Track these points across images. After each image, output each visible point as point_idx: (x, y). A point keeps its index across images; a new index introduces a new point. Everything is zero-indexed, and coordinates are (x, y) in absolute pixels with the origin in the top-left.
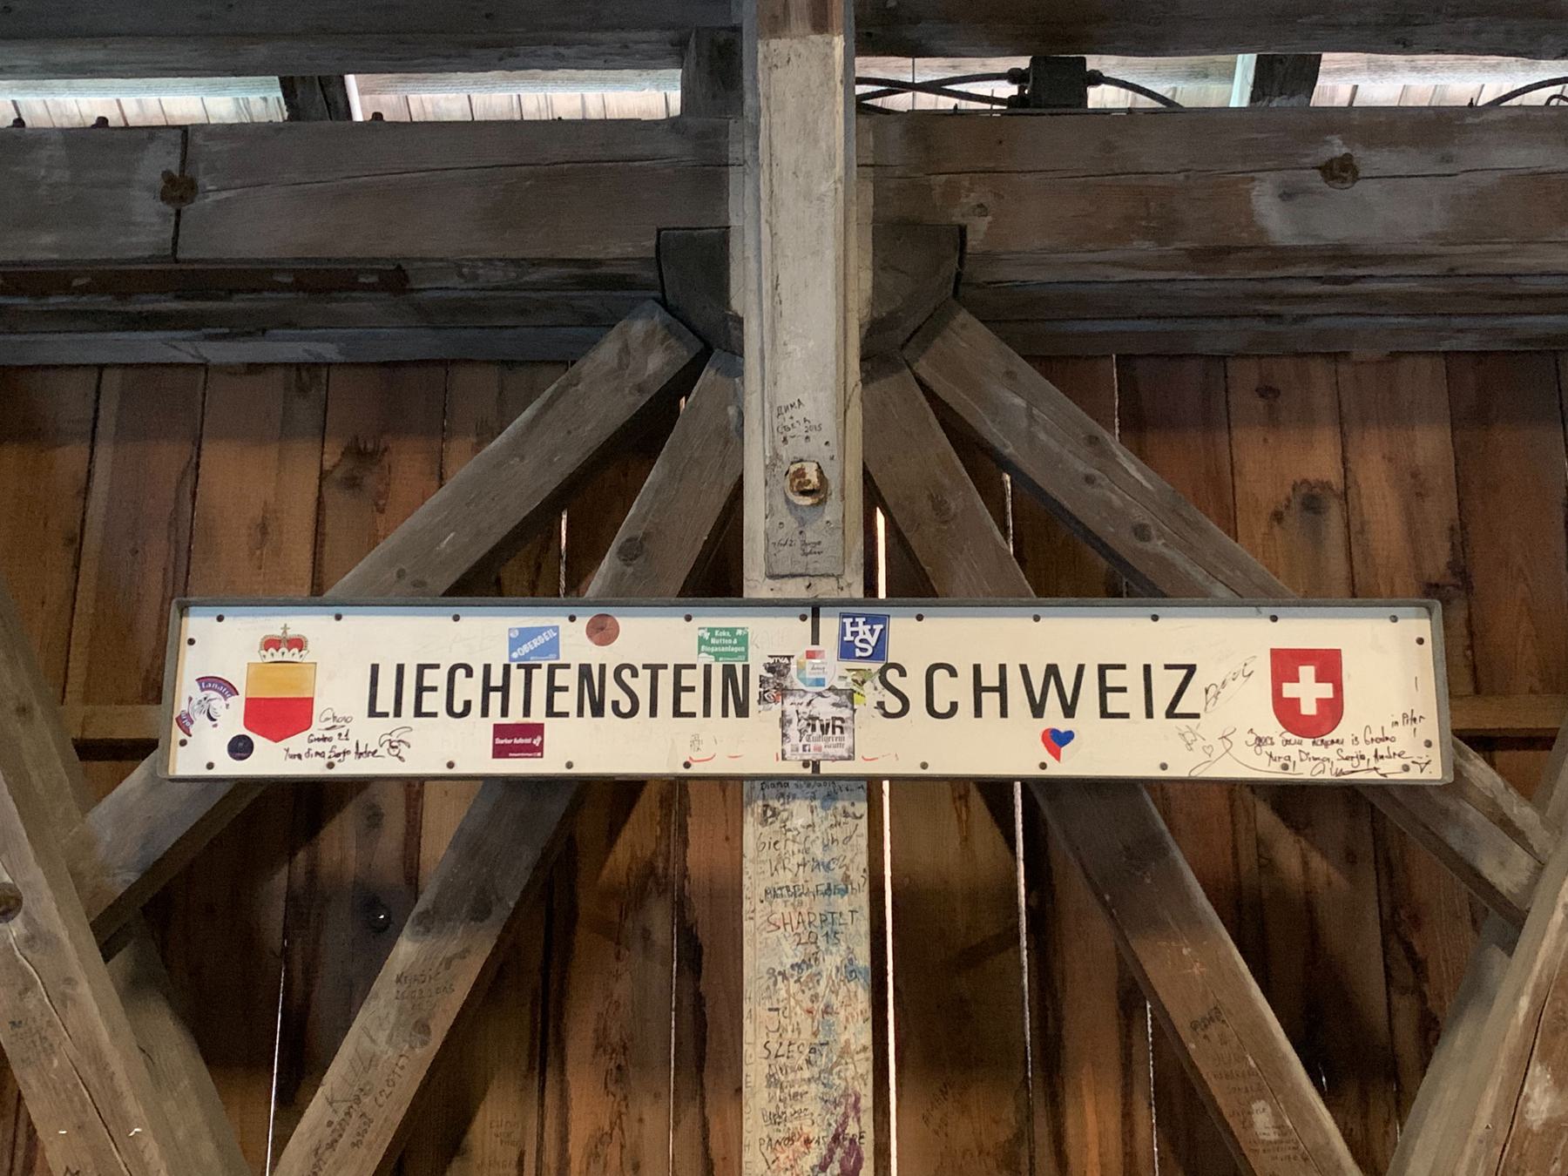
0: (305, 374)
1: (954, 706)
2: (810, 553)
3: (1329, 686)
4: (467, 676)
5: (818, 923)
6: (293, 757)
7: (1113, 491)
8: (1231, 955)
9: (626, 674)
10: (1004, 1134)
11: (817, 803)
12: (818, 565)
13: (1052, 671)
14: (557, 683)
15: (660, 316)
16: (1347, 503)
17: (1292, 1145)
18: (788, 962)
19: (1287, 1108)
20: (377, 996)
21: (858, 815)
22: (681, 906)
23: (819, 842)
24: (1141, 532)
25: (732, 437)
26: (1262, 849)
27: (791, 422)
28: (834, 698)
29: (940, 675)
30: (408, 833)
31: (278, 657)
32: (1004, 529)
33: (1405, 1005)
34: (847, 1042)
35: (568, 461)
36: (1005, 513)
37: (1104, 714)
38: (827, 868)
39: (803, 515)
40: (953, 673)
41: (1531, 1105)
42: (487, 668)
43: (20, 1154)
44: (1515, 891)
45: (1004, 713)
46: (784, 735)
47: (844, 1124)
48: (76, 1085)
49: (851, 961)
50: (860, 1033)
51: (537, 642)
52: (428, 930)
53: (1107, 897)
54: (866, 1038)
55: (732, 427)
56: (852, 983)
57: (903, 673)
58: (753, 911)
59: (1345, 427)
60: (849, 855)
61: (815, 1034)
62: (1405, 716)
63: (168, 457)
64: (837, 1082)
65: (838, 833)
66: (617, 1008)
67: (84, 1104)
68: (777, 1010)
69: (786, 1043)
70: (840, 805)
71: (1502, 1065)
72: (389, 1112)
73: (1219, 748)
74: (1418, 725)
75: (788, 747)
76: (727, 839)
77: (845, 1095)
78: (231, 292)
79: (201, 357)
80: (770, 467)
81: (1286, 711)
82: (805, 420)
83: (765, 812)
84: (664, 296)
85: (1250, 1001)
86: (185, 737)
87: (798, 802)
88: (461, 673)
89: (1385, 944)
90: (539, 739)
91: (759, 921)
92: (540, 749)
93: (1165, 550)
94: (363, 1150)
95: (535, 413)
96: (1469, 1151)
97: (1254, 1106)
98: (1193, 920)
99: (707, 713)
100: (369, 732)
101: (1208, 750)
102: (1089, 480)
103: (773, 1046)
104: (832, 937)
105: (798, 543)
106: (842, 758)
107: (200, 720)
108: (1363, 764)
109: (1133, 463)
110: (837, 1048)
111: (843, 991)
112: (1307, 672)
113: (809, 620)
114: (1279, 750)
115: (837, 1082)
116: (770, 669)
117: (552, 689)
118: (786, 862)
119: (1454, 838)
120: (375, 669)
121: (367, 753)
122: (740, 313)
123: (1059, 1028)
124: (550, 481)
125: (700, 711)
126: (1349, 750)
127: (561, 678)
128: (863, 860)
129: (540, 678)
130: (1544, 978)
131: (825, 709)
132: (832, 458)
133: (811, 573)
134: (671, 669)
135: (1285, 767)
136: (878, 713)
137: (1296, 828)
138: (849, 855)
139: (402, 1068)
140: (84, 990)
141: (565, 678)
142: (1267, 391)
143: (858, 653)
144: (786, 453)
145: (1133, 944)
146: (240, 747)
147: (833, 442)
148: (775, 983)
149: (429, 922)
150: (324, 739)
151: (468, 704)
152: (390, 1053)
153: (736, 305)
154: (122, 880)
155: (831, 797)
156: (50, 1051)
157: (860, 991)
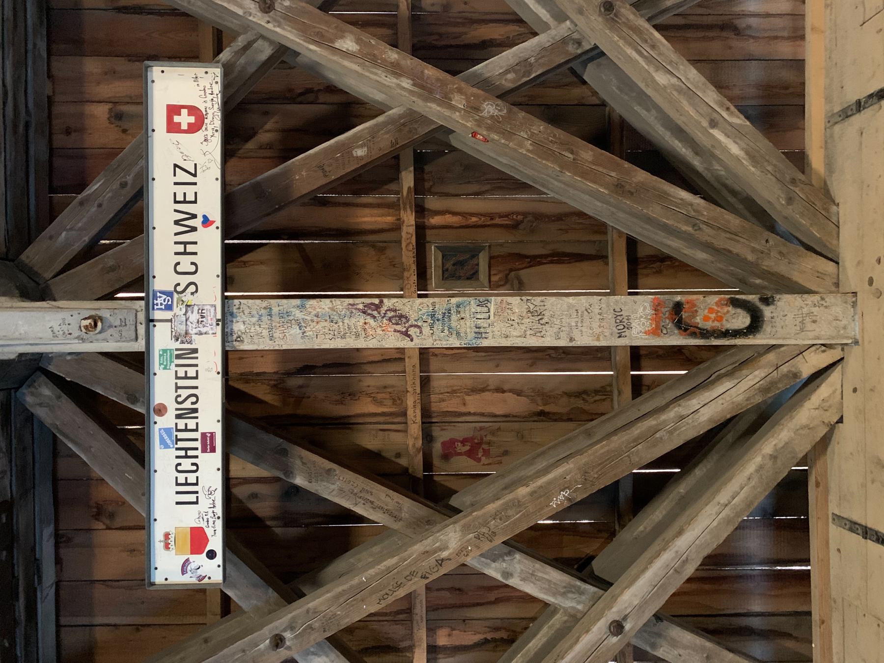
0: (59, 540)
1: (192, 263)
2: (125, 323)
3: (183, 110)
5: (283, 320)
6: (215, 533)
7: (105, 196)
8: (297, 160)
10: (372, 252)
11: (234, 320)
12: (131, 320)
13: (177, 223)
15: (24, 390)
16: (118, 102)
17: (368, 142)
18: (298, 331)
19: (355, 143)
20: (317, 490)
22: (289, 374)
23: (250, 319)
24: (124, 185)
25: (79, 356)
26: (263, 147)
27: (60, 330)
28: (189, 313)
29: (179, 269)
30: (260, 483)
31: (173, 543)
32: (124, 243)
33: (322, 98)
34: (329, 308)
35: (92, 427)
36: (116, 243)
37: (195, 202)
38: (261, 316)
40: (178, 263)
41: (350, 49)
42: (177, 457)
43: (381, 618)
44: (272, 48)
45: (195, 243)
46: (206, 333)
47: (359, 309)
48: (347, 604)
49: (298, 307)
51: (166, 437)
52: (292, 472)
53: (277, 207)
54: (327, 301)
55: (76, 357)
57: (178, 284)
58: (279, 345)
59: (84, 100)
60: (256, 307)
61: (326, 321)
62: (194, 81)
63: (99, 592)
64: (343, 312)
65: (246, 312)
66: (328, 397)
67: (355, 600)
69: (330, 332)
70: (235, 311)
71: (335, 58)
72: (360, 482)
73: (209, 156)
74: (199, 76)
75: (211, 332)
76: (262, 357)
77: (348, 309)
78: (14, 577)
79: (52, 584)
80: (83, 340)
81: (193, 128)
82: (60, 325)
83: (238, 341)
84: (14, 388)
85: (316, 154)
86: (207, 578)
87: (234, 328)
88: (179, 468)
89: (301, 103)
90: (207, 434)
91: (283, 343)
92: (212, 433)
93: (131, 176)
94: (373, 491)
96: (367, 74)
97: (355, 155)
98: (285, 174)
99: (196, 365)
100: (205, 503)
101: (210, 161)
102: (100, 206)
103: (331, 337)
104: (288, 314)
106: (215, 310)
107: (199, 572)
108: (214, 99)
109: (92, 187)
110: (331, 312)
111: (309, 310)
112: (176, 119)
113: (155, 323)
114: (210, 133)
115: (343, 312)
116: (177, 340)
117: (186, 430)
119: (252, 69)
120: (178, 503)
121: (214, 503)
122: (17, 355)
123: (334, 230)
124: (102, 435)
125: (195, 369)
126: (209, 104)
127: (181, 426)
128: (258, 301)
129: (181, 435)
130: (303, 38)
131: (194, 317)
132: (79, 314)
133: (134, 323)
134: (178, 381)
135: (217, 131)
136: (196, 295)
137: (255, 134)
138: (256, 307)
139: (344, 478)
140: (311, 605)
141: (181, 424)
142: (68, 132)
143: (170, 303)
144: (76, 333)
145: (295, 197)
146: (211, 555)
147: (71, 313)
148: (307, 336)
149: (288, 472)
150: (208, 521)
151: (193, 464)
152: (338, 483)
153: (12, 357)
154: (272, 594)
155: (232, 314)
156: (335, 615)
157: (309, 303)
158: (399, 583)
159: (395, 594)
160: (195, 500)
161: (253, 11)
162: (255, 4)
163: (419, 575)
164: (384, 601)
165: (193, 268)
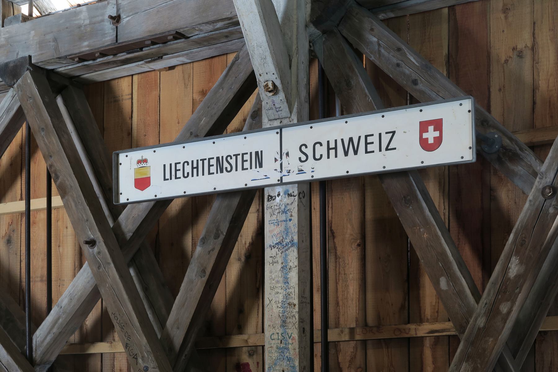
1: (321, 156)
3: (424, 137)
4: (306, 148)
9: (229, 158)
13: (351, 140)
14: (177, 169)
21: (295, 195)
23: (283, 205)
24: (415, 82)
29: (318, 146)
31: (141, 166)
37: (367, 152)
39: (273, 99)
40: (321, 145)
41: (510, 270)
42: (192, 161)
45: (336, 156)
49: (292, 241)
50: (295, 262)
56: (293, 247)
68: (272, 257)
83: (268, 197)
88: (186, 164)
95: (226, 72)
99: (251, 168)
102: (398, 65)
105: (274, 108)
112: (431, 128)
118: (274, 212)
120: (164, 165)
130: (519, 227)
134: (207, 159)
151: (188, 173)
157: (295, 249)
158: (124, 327)
159: (118, 325)
160: (178, 176)
161: (543, 181)
162: (549, 182)
163: (128, 342)
164: (114, 317)
165: (318, 156)
